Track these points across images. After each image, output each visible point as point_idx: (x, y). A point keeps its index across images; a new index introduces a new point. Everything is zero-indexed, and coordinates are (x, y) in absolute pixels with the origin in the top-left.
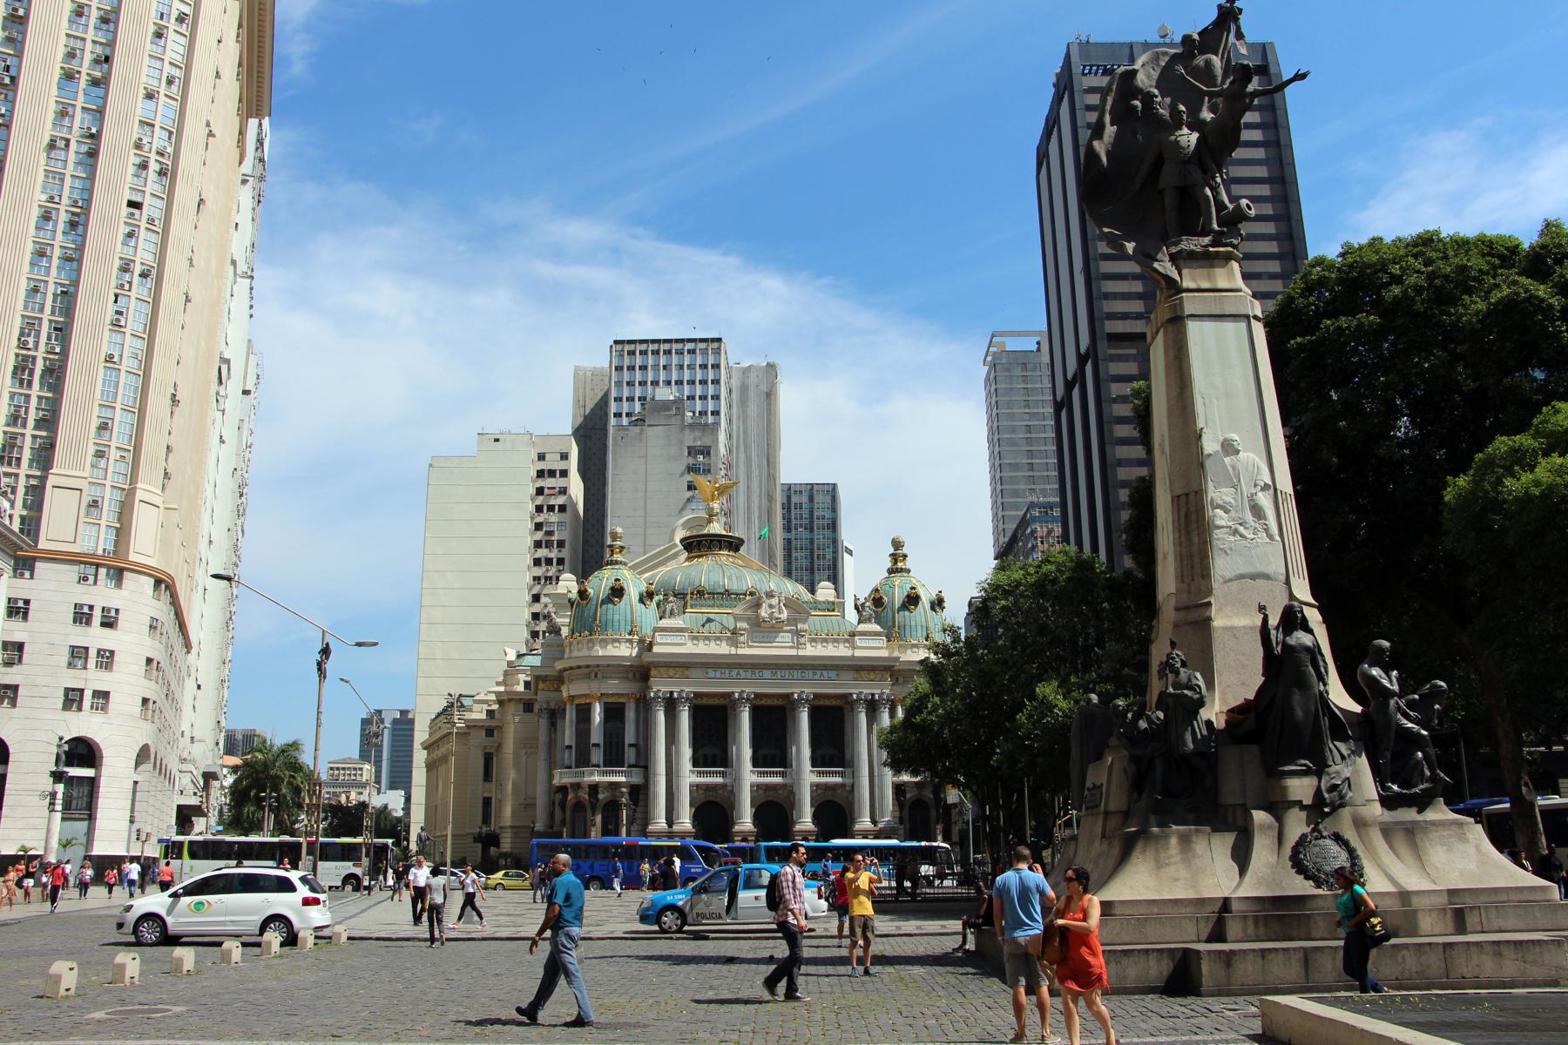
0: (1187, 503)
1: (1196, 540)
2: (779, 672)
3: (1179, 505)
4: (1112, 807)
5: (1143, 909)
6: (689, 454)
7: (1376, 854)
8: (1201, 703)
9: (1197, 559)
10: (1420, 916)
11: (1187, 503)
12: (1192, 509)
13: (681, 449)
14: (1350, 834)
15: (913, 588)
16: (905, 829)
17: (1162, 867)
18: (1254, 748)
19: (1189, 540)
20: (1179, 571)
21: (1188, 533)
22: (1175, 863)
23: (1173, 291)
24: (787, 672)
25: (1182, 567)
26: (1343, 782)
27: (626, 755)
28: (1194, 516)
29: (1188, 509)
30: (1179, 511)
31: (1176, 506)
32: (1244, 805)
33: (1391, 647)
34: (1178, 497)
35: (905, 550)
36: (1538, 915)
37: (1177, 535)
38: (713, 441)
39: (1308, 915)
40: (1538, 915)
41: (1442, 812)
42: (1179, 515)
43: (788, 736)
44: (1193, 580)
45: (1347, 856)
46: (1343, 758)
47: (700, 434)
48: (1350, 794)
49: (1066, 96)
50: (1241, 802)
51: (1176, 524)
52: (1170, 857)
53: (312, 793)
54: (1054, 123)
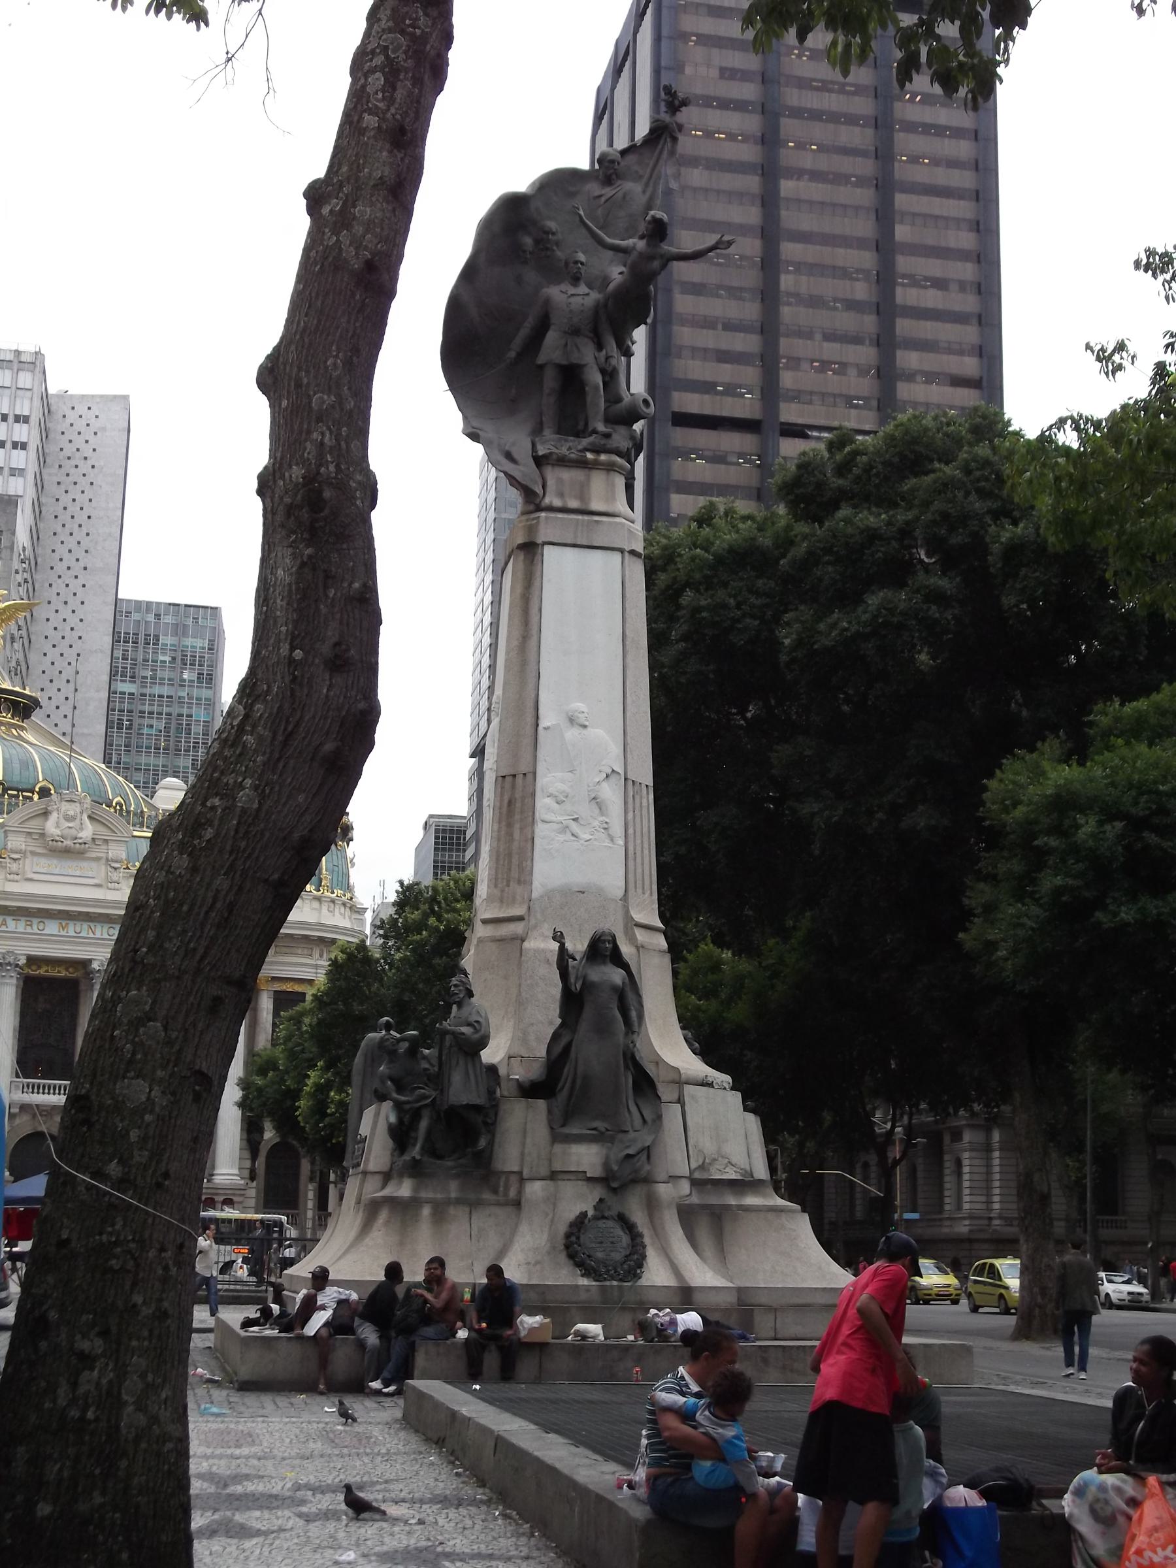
1: (517, 835)
2: (71, 924)
3: (502, 788)
4: (372, 1167)
8: (483, 1043)
9: (515, 860)
11: (513, 787)
12: (518, 795)
14: (639, 1217)
16: (257, 1188)
18: (541, 1104)
19: (510, 835)
20: (493, 872)
23: (532, 507)
24: (85, 926)
25: (497, 869)
27: (651, 797)
28: (518, 805)
30: (502, 795)
31: (499, 786)
32: (520, 1173)
34: (504, 777)
37: (496, 827)
44: (508, 885)
45: (629, 1241)
46: (644, 1121)
48: (647, 1167)
49: (649, 11)
50: (516, 1169)
51: (497, 812)
53: (278, 1299)
54: (627, 53)
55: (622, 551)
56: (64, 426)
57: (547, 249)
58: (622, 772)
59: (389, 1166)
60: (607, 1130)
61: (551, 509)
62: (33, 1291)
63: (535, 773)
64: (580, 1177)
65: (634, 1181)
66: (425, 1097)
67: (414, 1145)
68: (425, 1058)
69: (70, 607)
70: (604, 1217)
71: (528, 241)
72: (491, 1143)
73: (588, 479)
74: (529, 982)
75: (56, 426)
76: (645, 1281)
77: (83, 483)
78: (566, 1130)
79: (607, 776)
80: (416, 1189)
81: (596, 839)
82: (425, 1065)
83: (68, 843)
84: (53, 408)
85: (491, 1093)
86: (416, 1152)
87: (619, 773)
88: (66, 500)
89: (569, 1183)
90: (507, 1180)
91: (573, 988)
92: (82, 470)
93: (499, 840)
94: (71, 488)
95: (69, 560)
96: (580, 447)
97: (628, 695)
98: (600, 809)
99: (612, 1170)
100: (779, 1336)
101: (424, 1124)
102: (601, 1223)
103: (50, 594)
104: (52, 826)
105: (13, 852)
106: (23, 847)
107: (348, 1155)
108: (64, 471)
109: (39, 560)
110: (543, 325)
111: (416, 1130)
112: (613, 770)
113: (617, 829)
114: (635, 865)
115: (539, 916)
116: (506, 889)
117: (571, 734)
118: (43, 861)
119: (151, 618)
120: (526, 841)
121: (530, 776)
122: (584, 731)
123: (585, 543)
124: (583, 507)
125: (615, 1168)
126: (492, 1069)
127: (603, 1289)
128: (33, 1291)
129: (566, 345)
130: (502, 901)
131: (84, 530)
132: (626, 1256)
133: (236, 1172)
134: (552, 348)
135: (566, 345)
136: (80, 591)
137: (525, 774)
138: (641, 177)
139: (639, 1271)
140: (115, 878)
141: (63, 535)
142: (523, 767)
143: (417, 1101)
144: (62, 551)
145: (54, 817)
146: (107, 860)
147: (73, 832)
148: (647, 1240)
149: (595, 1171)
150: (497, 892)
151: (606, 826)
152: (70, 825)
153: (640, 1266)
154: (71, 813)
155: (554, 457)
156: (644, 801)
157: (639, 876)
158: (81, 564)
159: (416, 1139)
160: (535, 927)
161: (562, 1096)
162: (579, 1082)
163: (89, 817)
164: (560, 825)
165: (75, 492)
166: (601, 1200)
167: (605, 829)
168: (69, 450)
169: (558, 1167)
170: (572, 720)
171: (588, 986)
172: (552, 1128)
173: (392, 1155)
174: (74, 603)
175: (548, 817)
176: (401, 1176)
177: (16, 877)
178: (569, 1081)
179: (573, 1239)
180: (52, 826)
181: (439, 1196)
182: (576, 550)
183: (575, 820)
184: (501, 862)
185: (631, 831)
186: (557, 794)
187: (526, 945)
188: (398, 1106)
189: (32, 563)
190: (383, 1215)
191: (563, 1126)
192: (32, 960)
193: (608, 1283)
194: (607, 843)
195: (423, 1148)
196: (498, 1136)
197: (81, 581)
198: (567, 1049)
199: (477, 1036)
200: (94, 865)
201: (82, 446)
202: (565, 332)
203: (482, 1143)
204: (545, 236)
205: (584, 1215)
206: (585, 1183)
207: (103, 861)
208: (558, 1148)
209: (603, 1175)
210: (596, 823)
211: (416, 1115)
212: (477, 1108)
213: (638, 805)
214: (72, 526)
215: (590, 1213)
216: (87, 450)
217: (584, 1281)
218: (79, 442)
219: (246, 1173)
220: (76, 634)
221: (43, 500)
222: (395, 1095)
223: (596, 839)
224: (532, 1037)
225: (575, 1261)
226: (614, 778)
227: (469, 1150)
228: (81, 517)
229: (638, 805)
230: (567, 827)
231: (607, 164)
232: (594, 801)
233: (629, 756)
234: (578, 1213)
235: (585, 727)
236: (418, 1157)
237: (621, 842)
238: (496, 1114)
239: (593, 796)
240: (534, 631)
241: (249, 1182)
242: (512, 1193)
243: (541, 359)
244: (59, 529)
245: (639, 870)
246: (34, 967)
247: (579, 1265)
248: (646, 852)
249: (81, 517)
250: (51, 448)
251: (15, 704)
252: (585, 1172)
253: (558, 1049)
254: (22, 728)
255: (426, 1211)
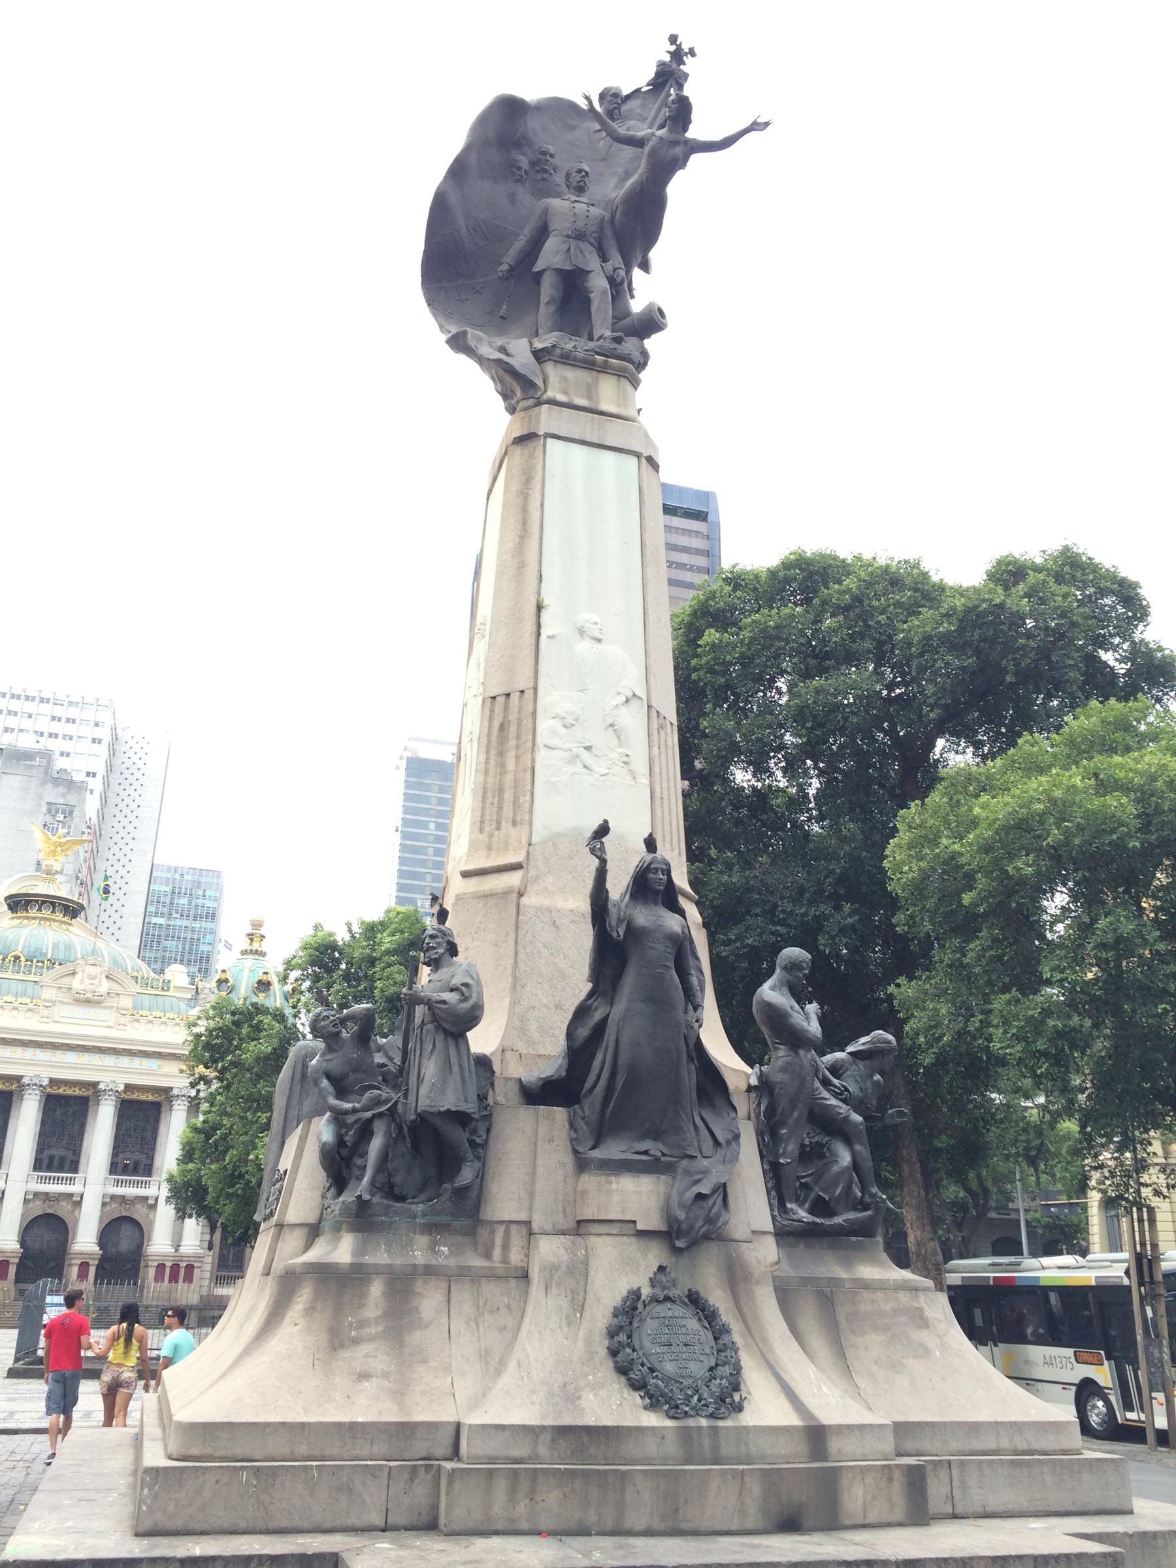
0: (506, 708)
1: (511, 765)
3: (492, 711)
4: (292, 1216)
5: (277, 1445)
6: (49, 811)
7: (765, 1340)
8: (472, 1018)
9: (508, 796)
10: (845, 1481)
11: (506, 708)
12: (513, 717)
13: (39, 805)
14: (717, 1297)
15: (266, 973)
16: (213, 1256)
17: (342, 1346)
18: (560, 1114)
19: (502, 766)
20: (478, 813)
21: (501, 754)
22: (371, 1339)
25: (483, 809)
26: (714, 1191)
28: (513, 729)
29: (505, 716)
30: (491, 719)
32: (528, 1223)
33: (813, 961)
34: (494, 698)
35: (263, 931)
36: (1048, 1479)
38: (79, 801)
39: (624, 1473)
40: (1048, 1479)
41: (881, 1265)
42: (490, 727)
43: (86, 1135)
44: (498, 828)
46: (717, 1143)
47: (65, 791)
50: (523, 1216)
52: (362, 1324)
55: (638, 455)
56: (126, 748)
57: (545, 171)
58: (644, 696)
59: (318, 1213)
60: (664, 1155)
61: (553, 402)
62: (1039, 1072)
63: (535, 689)
64: (628, 1228)
65: (707, 1237)
66: (378, 1102)
67: (360, 1178)
68: (380, 1049)
69: (121, 863)
70: (667, 1299)
71: (524, 162)
72: (481, 1176)
73: (597, 380)
74: (528, 950)
75: (120, 748)
76: (750, 1417)
77: (136, 784)
78: (596, 1154)
79: (627, 701)
80: (359, 1251)
81: (614, 774)
82: (379, 1058)
83: (89, 995)
84: (119, 737)
85: (482, 1098)
86: (361, 1187)
87: (640, 698)
88: (123, 795)
89: (608, 1239)
90: (507, 1236)
91: (614, 934)
92: (136, 776)
93: (486, 773)
94: (128, 787)
95: (123, 833)
96: (586, 348)
97: (650, 612)
98: (619, 737)
99: (677, 1220)
100: (959, 1510)
101: (376, 1145)
102: (662, 1309)
103: (109, 854)
104: (77, 983)
105: (45, 1001)
106: (54, 998)
107: (261, 1206)
108: (124, 776)
109: (103, 832)
110: (542, 233)
111: (364, 1155)
112: (634, 695)
113: (641, 766)
114: (663, 812)
115: (541, 864)
116: (496, 833)
117: (584, 647)
118: (67, 1008)
119: (177, 876)
120: (525, 770)
121: (529, 694)
122: (598, 646)
123: (596, 441)
124: (593, 406)
125: (682, 1215)
126: (483, 1062)
127: (686, 1435)
128: (1039, 1072)
129: (569, 249)
130: (490, 849)
131: (135, 814)
132: (711, 1369)
133: (198, 1243)
134: (552, 255)
135: (569, 249)
136: (129, 853)
137: (522, 692)
138: (645, 119)
139: (737, 1397)
140: (123, 1022)
141: (120, 817)
142: (523, 682)
143: (366, 1109)
144: (118, 827)
145: (79, 977)
146: (118, 1008)
147: (93, 987)
148: (737, 1337)
149: (652, 1221)
150: (483, 838)
151: (625, 759)
152: (92, 982)
153: (736, 1388)
154: (93, 973)
155: (558, 351)
156: (669, 739)
157: (667, 828)
158: (131, 836)
159: (364, 1168)
160: (536, 879)
161: (591, 1105)
162: (620, 1080)
163: (107, 977)
164: (569, 753)
165: (130, 790)
166: (661, 1269)
167: (626, 763)
168: (128, 763)
169: (588, 1213)
170: (581, 632)
171: (634, 933)
172: (575, 1152)
173: (323, 1197)
174: (124, 860)
175: (555, 742)
176: (337, 1228)
177: (46, 1020)
178: (605, 1075)
179: (622, 1337)
180: (77, 983)
181: (399, 1261)
182: (585, 447)
183: (588, 748)
184: (489, 800)
185: (656, 769)
186: (565, 715)
187: (525, 900)
188: (339, 1118)
189: (96, 833)
190: (304, 1297)
191: (593, 1148)
192: (53, 1082)
193: (691, 1423)
194: (628, 779)
195: (373, 1183)
196: (491, 1162)
197: (129, 847)
198: (600, 1029)
199: (466, 1005)
200: (107, 1012)
201: (137, 761)
202: (569, 237)
203: (466, 1175)
204: (542, 157)
205: (635, 1294)
206: (633, 1240)
207: (115, 1009)
208: (589, 1181)
209: (663, 1227)
210: (613, 755)
211: (365, 1131)
212: (460, 1118)
213: (662, 742)
214: (126, 811)
215: (646, 1292)
216: (140, 764)
217: (652, 1420)
218: (135, 758)
219: (206, 1244)
220: (124, 880)
221: (108, 794)
222: (333, 1101)
223: (614, 774)
224: (533, 1026)
225: (629, 1380)
226: (634, 703)
227: (447, 1186)
228: (133, 806)
229: (662, 742)
230: (578, 756)
231: (609, 98)
232: (611, 728)
233: (652, 681)
234: (625, 1293)
235: (599, 640)
236: (366, 1197)
237: (645, 781)
238: (488, 1131)
239: (610, 721)
240: (535, 529)
241: (207, 1251)
242: (516, 1257)
243: (539, 266)
244: (118, 813)
245: (667, 821)
246: (55, 1088)
247: (637, 1386)
248: (673, 800)
249: (133, 806)
250: (117, 762)
251: (66, 908)
252: (634, 1222)
253: (583, 1032)
254: (70, 924)
255: (376, 1289)
